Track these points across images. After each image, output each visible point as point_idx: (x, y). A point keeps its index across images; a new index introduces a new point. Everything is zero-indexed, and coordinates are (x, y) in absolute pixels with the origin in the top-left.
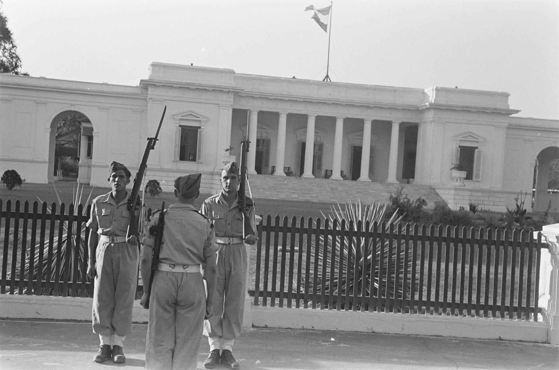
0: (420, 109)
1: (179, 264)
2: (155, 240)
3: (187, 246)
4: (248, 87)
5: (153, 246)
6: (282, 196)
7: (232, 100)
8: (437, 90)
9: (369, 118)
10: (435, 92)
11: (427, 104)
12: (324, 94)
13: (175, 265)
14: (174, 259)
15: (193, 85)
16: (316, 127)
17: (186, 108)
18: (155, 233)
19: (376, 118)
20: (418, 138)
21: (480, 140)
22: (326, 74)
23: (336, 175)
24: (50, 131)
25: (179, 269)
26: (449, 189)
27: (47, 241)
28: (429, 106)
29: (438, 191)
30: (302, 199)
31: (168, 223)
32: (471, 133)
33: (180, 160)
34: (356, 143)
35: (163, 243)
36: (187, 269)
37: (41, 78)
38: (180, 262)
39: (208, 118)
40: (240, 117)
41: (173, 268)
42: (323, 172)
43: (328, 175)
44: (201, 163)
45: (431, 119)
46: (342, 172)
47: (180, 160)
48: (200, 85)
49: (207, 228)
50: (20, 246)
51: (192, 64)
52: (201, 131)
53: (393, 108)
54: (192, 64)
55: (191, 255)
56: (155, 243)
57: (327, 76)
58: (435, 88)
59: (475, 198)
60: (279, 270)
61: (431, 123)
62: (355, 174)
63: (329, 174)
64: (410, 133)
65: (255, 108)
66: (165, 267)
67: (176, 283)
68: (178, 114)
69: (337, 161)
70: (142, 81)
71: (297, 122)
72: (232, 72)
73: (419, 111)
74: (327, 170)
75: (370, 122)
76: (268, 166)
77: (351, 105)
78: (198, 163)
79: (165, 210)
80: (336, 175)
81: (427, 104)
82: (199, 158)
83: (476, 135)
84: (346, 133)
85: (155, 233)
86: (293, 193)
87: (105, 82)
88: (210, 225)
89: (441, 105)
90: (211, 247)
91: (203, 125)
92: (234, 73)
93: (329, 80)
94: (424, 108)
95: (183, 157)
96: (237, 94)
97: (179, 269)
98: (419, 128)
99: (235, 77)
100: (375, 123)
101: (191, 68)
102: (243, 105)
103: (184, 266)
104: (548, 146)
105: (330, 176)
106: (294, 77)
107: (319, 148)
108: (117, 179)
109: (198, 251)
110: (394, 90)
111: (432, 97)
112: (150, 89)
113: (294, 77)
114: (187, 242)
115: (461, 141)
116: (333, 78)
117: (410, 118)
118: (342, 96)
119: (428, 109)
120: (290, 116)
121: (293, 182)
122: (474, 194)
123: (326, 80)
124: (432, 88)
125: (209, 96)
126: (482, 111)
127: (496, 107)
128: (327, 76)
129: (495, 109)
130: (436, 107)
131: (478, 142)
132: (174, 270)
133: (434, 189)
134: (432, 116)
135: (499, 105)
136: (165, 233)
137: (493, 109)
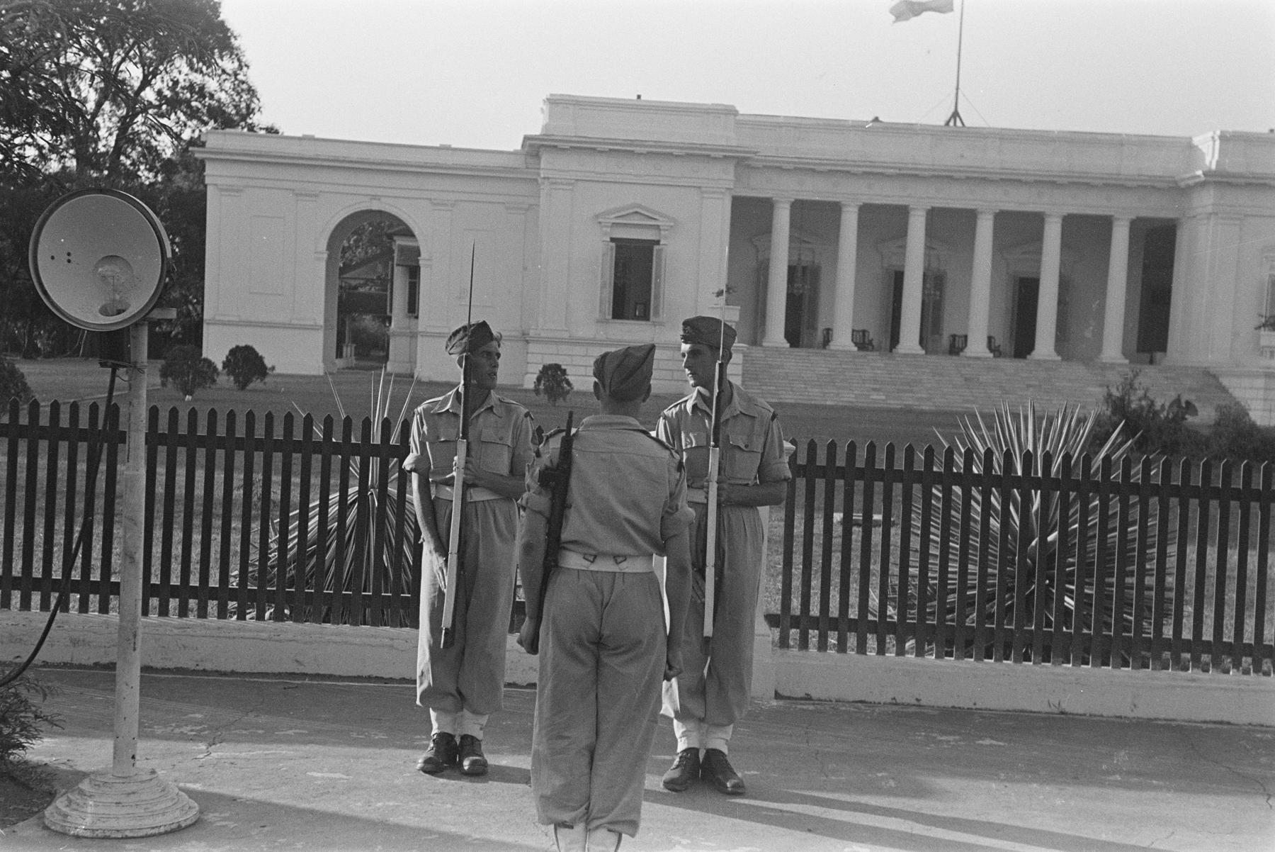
0: (1182, 184)
1: (604, 555)
2: (552, 499)
4: (767, 147)
5: (547, 514)
6: (848, 397)
7: (731, 176)
8: (1224, 138)
10: (1218, 142)
11: (1199, 173)
12: (949, 156)
13: (595, 557)
14: (593, 542)
15: (642, 143)
16: (1065, 245)
18: (552, 484)
19: (1144, 213)
22: (952, 110)
23: (977, 346)
24: (325, 256)
26: (1256, 376)
27: (315, 503)
28: (1203, 178)
29: (1225, 382)
30: (894, 404)
32: (640, 206)
34: (1025, 270)
36: (624, 565)
38: (608, 548)
39: (674, 220)
40: (750, 218)
42: (945, 341)
43: (957, 346)
44: (661, 324)
45: (1210, 209)
46: (990, 339)
48: (657, 144)
50: (198, 507)
51: (639, 97)
52: (660, 251)
53: (1115, 185)
54: (639, 97)
55: (632, 532)
56: (553, 507)
57: (956, 115)
58: (1218, 133)
61: (1208, 219)
63: (959, 343)
64: (1157, 246)
66: (573, 561)
69: (980, 313)
70: (526, 138)
71: (884, 224)
72: (731, 112)
73: (1180, 190)
74: (954, 336)
75: (788, 206)
76: (815, 329)
78: (654, 324)
79: (573, 431)
80: (977, 346)
81: (1199, 173)
82: (657, 313)
83: (656, 213)
84: (1001, 246)
86: (874, 390)
87: (446, 143)
89: (1234, 176)
91: (666, 238)
92: (735, 113)
93: (959, 124)
94: (1191, 182)
96: (742, 162)
98: (1179, 233)
99: (738, 123)
102: (759, 187)
105: (962, 350)
106: (876, 119)
107: (935, 283)
109: (646, 519)
110: (1117, 142)
111: (1210, 156)
113: (876, 119)
114: (624, 504)
116: (970, 119)
117: (1156, 208)
118: (991, 159)
119: (1203, 184)
121: (875, 363)
123: (952, 124)
124: (1211, 134)
128: (956, 115)
130: (1220, 180)
132: (594, 568)
133: (1214, 376)
134: (1212, 201)
136: (574, 483)
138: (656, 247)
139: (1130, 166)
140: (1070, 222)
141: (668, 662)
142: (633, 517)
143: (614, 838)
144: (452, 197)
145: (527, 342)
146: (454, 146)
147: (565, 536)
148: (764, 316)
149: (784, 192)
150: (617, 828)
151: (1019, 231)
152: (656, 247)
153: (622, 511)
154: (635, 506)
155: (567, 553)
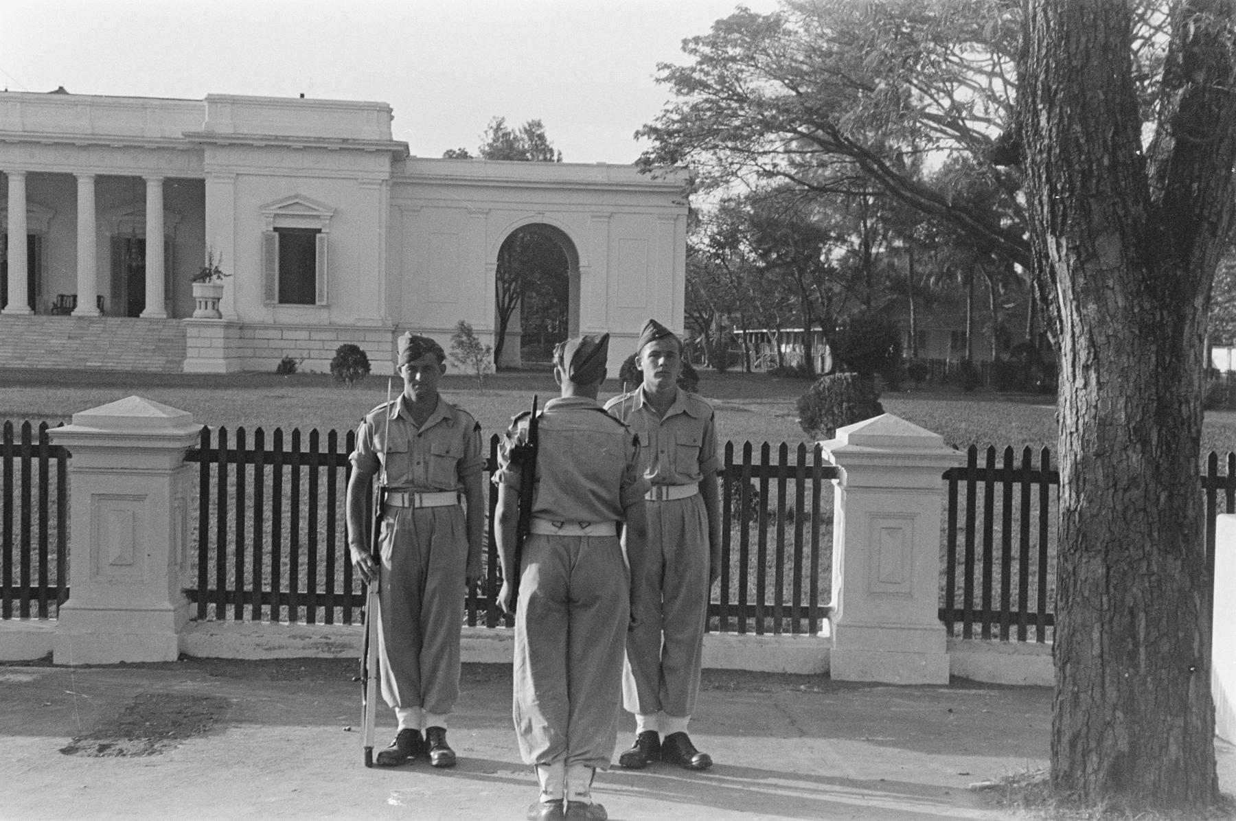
1: (571, 522)
2: (522, 475)
3: (583, 481)
5: (518, 487)
7: (387, 168)
9: (85, 170)
13: (563, 523)
14: (560, 511)
16: (167, 207)
17: (284, 189)
18: (521, 461)
19: (32, 169)
20: (93, 206)
21: (322, 212)
23: (86, 306)
25: (572, 531)
31: (545, 444)
33: (281, 302)
35: (538, 481)
36: (588, 529)
37: (600, 165)
38: (573, 516)
41: (560, 528)
43: (65, 306)
46: (99, 298)
47: (281, 302)
49: (626, 447)
51: (302, 96)
54: (302, 96)
56: (523, 481)
59: (319, 345)
60: (998, 527)
62: (135, 306)
63: (68, 303)
64: (187, 198)
65: (85, 170)
66: (543, 527)
67: (566, 557)
68: (274, 203)
69: (86, 274)
70: (406, 146)
74: (62, 296)
77: (30, 143)
79: (538, 413)
80: (86, 306)
83: (314, 202)
84: (102, 207)
85: (521, 461)
87: (602, 160)
88: (630, 439)
90: (635, 485)
95: (287, 296)
97: (572, 531)
100: (168, 184)
101: (302, 104)
103: (582, 524)
104: (562, 227)
106: (61, 90)
108: (661, 361)
109: (609, 491)
110: (142, 105)
112: (208, 153)
113: (61, 90)
114: (587, 476)
115: (276, 216)
117: (181, 168)
120: (32, 179)
122: (315, 336)
125: (330, 163)
126: (316, 147)
127: (345, 137)
129: (345, 140)
131: (318, 217)
132: (561, 533)
135: (367, 132)
136: (540, 460)
137: (361, 142)
138: (318, 236)
139: (154, 129)
140: (168, 184)
141: (631, 616)
142: (595, 488)
143: (589, 772)
144: (486, 206)
145: (393, 332)
146: (608, 162)
147: (537, 507)
148: (167, 290)
149: (153, 172)
150: (592, 763)
151: (120, 194)
152: (318, 236)
153: (583, 481)
154: (595, 478)
155: (537, 521)
